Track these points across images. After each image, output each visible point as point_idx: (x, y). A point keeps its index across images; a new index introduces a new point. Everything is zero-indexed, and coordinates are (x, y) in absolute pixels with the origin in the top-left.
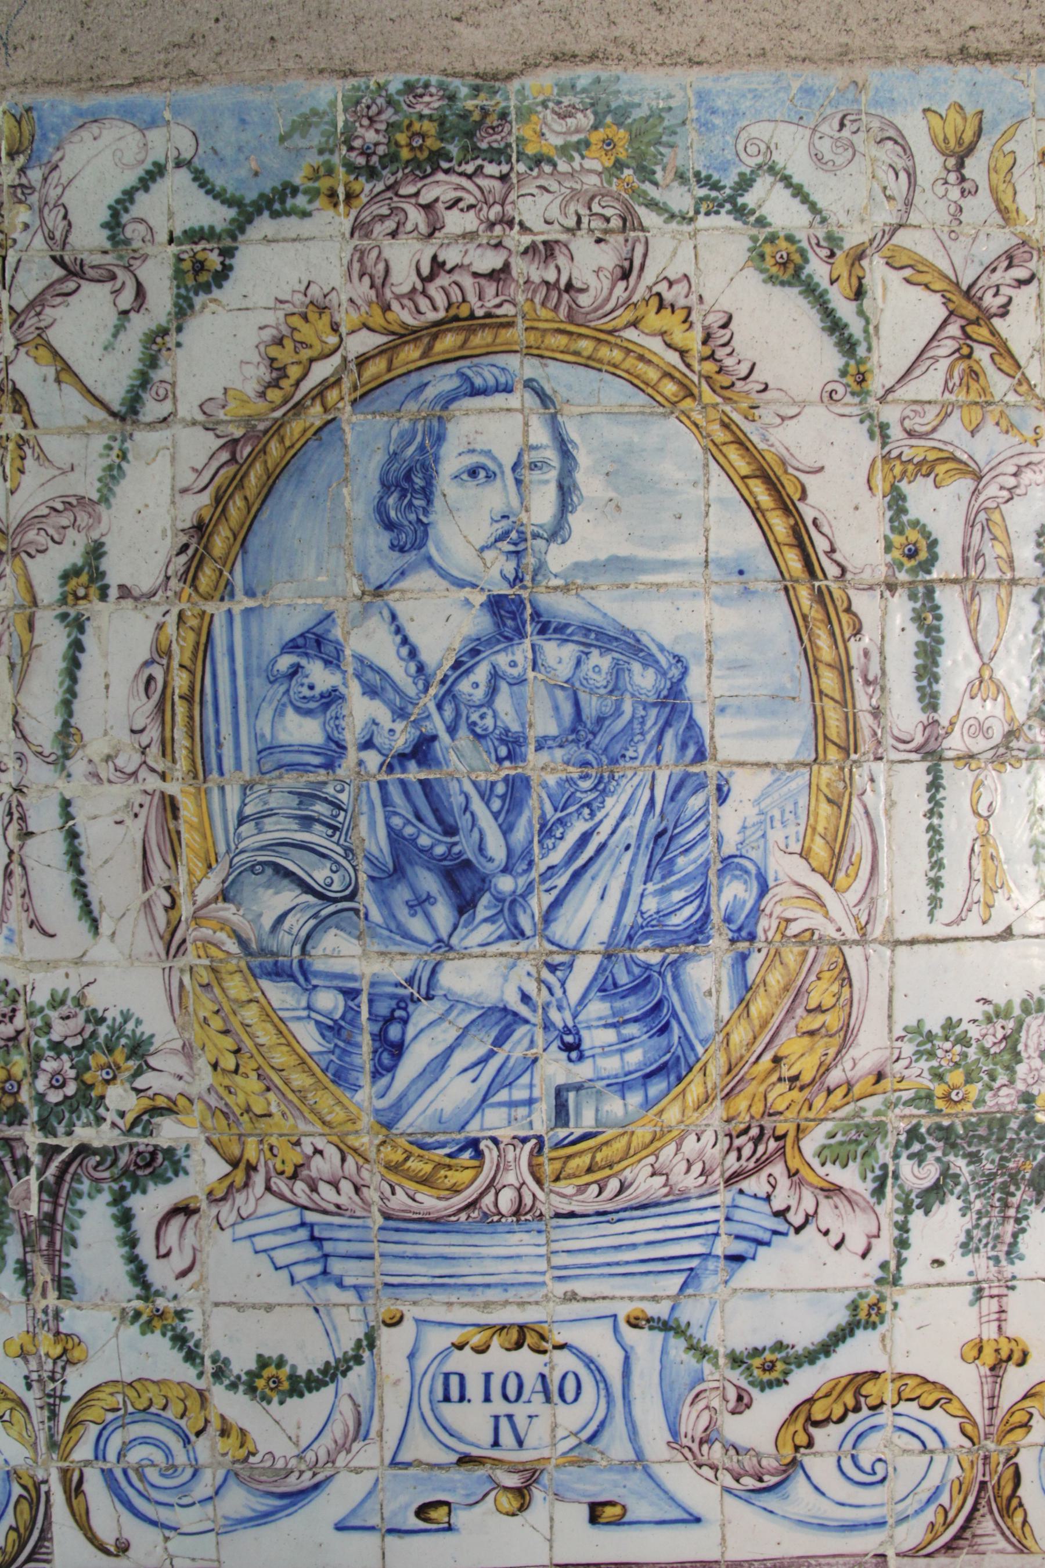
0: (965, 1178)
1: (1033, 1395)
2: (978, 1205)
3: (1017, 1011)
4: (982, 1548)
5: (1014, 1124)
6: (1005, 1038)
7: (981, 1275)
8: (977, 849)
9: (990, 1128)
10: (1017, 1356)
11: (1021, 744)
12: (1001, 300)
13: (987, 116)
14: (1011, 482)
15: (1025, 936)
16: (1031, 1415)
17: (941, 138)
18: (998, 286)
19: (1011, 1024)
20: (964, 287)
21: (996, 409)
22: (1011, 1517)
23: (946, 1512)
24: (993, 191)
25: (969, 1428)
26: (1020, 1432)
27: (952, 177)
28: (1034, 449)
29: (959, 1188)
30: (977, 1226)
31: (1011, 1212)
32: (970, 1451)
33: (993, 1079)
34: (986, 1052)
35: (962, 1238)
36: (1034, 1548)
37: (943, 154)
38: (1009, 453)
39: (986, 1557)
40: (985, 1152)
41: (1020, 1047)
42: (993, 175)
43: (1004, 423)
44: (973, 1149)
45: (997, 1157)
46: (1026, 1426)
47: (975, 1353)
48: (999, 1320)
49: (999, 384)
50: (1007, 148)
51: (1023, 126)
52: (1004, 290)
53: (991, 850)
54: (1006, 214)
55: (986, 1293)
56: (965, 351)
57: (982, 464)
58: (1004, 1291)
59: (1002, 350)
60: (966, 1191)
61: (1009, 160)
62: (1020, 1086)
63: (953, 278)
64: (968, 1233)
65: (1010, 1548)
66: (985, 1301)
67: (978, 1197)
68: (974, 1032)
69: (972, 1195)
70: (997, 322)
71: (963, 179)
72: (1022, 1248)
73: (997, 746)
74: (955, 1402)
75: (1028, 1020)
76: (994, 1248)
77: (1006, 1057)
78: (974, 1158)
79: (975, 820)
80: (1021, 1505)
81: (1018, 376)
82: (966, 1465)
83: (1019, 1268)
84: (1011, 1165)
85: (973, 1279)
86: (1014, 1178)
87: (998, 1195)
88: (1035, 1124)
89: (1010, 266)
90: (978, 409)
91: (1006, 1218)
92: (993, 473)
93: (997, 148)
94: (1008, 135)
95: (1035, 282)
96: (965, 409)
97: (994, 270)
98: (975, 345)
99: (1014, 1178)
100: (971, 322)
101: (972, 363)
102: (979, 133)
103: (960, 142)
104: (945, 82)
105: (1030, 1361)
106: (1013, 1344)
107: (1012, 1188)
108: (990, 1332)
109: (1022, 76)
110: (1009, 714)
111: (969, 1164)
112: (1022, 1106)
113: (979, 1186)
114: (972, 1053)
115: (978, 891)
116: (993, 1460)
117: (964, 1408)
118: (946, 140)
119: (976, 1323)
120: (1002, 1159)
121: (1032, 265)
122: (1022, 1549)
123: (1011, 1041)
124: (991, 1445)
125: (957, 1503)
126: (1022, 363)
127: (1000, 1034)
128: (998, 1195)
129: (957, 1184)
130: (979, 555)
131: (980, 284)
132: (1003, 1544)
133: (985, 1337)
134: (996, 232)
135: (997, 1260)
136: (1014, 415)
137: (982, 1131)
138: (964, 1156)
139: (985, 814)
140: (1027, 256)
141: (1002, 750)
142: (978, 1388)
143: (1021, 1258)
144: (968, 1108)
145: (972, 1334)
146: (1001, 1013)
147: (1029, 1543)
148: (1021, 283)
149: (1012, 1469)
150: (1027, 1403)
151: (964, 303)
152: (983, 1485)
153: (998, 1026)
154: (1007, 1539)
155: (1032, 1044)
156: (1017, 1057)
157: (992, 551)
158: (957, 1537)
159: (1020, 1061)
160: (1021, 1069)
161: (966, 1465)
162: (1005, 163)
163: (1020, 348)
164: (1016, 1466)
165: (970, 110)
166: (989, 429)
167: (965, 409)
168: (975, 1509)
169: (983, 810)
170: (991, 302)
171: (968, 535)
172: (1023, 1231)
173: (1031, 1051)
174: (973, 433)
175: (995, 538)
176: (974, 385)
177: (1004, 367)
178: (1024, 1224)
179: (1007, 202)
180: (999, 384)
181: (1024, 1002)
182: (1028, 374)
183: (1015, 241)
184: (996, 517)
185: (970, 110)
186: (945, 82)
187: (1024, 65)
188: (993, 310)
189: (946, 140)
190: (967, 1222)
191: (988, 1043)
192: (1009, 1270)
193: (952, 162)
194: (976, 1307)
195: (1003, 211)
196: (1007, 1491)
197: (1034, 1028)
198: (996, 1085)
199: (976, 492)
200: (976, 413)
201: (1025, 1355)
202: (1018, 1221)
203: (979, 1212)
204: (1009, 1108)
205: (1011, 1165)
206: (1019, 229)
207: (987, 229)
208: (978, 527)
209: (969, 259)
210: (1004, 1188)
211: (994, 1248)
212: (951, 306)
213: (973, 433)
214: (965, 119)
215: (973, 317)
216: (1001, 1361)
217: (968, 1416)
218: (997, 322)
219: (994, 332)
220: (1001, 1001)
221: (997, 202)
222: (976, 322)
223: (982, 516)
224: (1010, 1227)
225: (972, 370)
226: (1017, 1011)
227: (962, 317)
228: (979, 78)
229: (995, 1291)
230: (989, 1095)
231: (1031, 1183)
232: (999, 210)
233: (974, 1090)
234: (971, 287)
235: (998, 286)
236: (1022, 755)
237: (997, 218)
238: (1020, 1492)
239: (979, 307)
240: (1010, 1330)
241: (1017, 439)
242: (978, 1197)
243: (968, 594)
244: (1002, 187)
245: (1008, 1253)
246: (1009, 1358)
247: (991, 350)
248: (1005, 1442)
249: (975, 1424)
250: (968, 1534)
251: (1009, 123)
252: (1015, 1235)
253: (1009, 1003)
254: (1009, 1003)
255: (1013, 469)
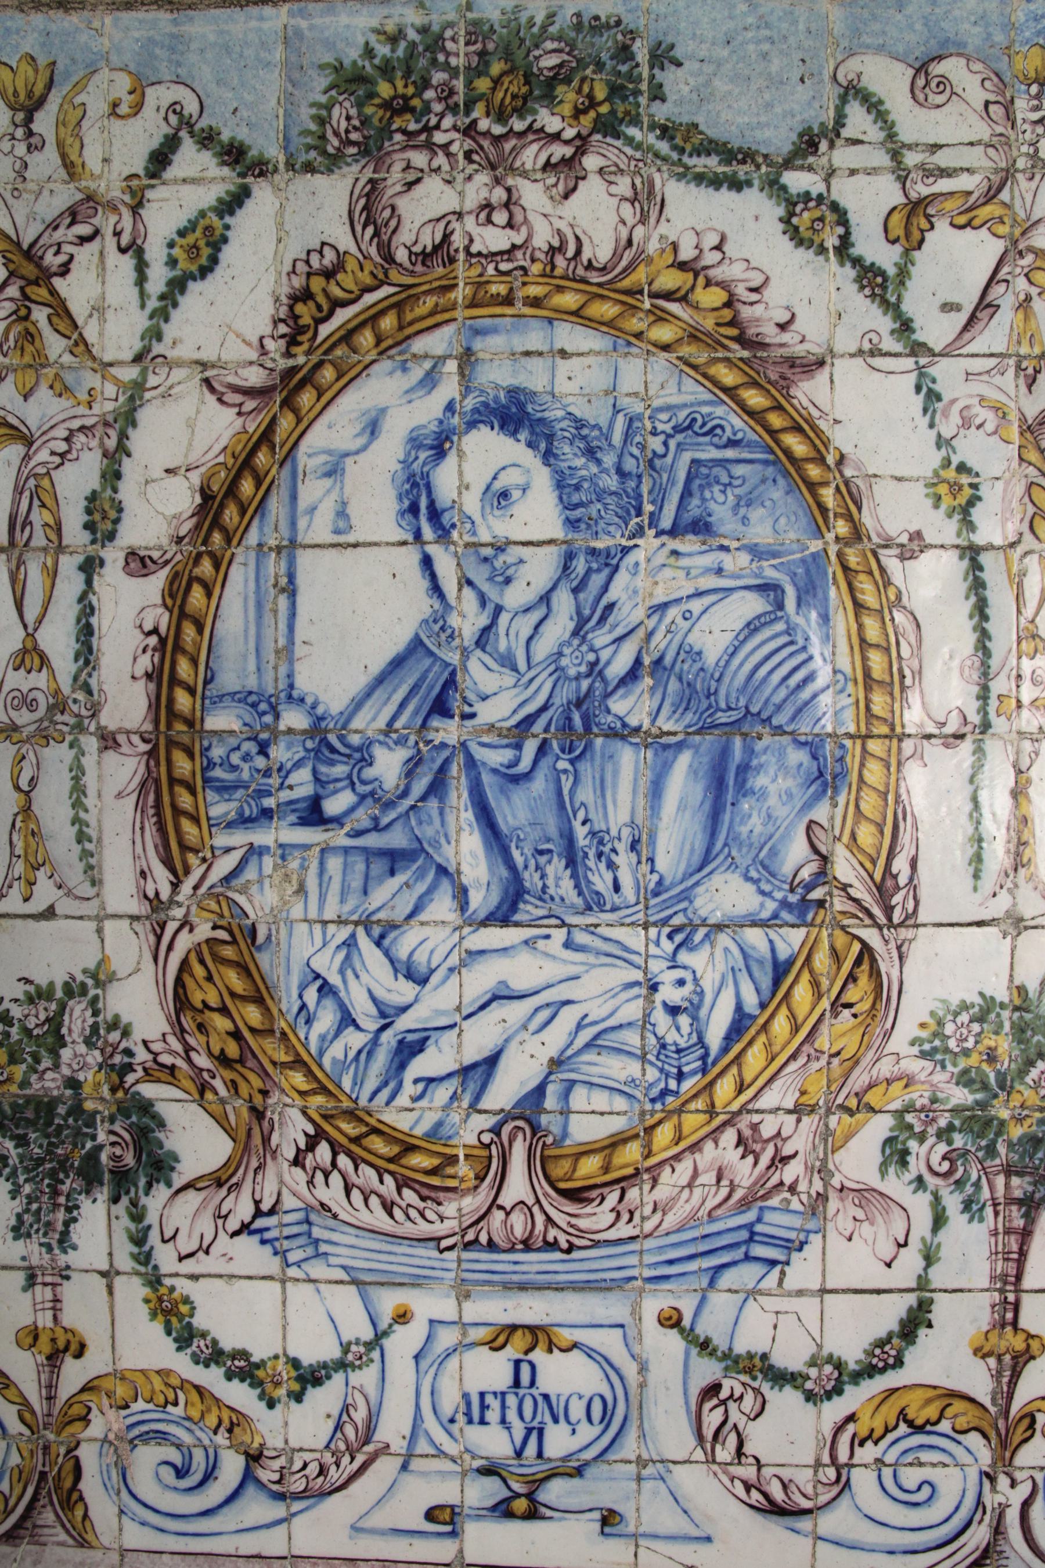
0: (14, 1160)
1: (91, 1389)
2: (27, 1189)
3: (59, 994)
4: (43, 1539)
5: (62, 1110)
6: (48, 1020)
7: (35, 1261)
8: (18, 824)
9: (37, 1111)
10: (74, 1347)
11: (66, 718)
12: (62, 258)
13: (60, 67)
14: (62, 447)
15: (67, 917)
16: (90, 1409)
17: (10, 91)
18: (59, 245)
19: (53, 1006)
20: (25, 246)
21: (50, 372)
22: (72, 1509)
23: (6, 1500)
24: (60, 145)
25: (27, 1416)
26: (79, 1425)
27: (20, 133)
28: (87, 412)
29: (7, 1170)
30: (27, 1211)
31: (62, 1200)
32: (29, 1440)
33: (37, 1060)
34: (27, 1032)
35: (13, 1222)
36: (95, 1543)
37: (12, 108)
38: (61, 417)
39: (47, 1549)
40: (33, 1136)
41: (64, 1031)
42: (62, 129)
43: (58, 386)
44: (21, 1131)
45: (45, 1143)
46: (85, 1419)
47: (29, 1340)
48: (54, 1308)
49: (55, 345)
50: (78, 100)
51: (96, 78)
52: (67, 248)
53: (32, 826)
54: (71, 169)
55: (39, 1280)
56: (23, 312)
57: (33, 429)
58: (58, 1280)
59: (60, 310)
60: (14, 1173)
61: (79, 112)
62: (66, 1071)
63: (12, 233)
64: (19, 1216)
65: (71, 1541)
66: (38, 1288)
67: (26, 1181)
68: (16, 1012)
69: (21, 1179)
70: (57, 282)
71: (30, 134)
72: (74, 1238)
73: (41, 720)
74: (13, 1389)
75: (71, 1003)
76: (45, 1234)
77: (50, 1040)
78: (22, 1141)
79: (16, 795)
80: (81, 1498)
81: (75, 336)
82: (26, 1454)
83: (72, 1258)
84: (60, 1151)
85: (26, 1264)
86: (63, 1164)
87: (47, 1181)
88: (83, 1111)
89: (72, 223)
90: (31, 372)
91: (56, 1206)
92: (45, 438)
93: (67, 100)
94: (80, 86)
95: (98, 239)
96: (20, 373)
97: (56, 228)
98: (33, 306)
99: (63, 1164)
100: (30, 283)
101: (28, 325)
102: (50, 85)
103: (30, 94)
104: (18, 32)
105: (88, 1354)
106: (70, 1335)
107: (61, 1176)
108: (45, 1320)
109: (96, 24)
110: (53, 686)
111: (16, 1147)
112: (69, 1092)
113: (27, 1170)
114: (14, 1031)
115: (19, 868)
116: (54, 1448)
117: (21, 1394)
118: (16, 93)
119: (30, 1310)
120: (50, 1144)
121: (96, 221)
122: (82, 1543)
123: (55, 1023)
124: (51, 1437)
125: (17, 1491)
126: (80, 323)
127: (42, 1016)
128: (47, 1181)
129: (6, 1165)
130: (27, 522)
131: (41, 242)
132: (63, 1537)
133: (40, 1324)
134: (57, 186)
135: (49, 1248)
136: (69, 378)
137: (30, 1114)
138: (12, 1138)
139: (26, 788)
140: (91, 212)
141: (46, 724)
142: (35, 1376)
143: (75, 1248)
144: (14, 1089)
145: (28, 1321)
146: (39, 995)
147: (90, 1537)
148: (83, 240)
149: (72, 1462)
150: (85, 1397)
151: (25, 263)
152: (43, 1475)
153: (41, 1008)
154: (67, 1532)
155: (76, 1028)
156: (61, 1042)
157: (39, 517)
158: (18, 1525)
159: (64, 1045)
160: (66, 1054)
161: (26, 1454)
162: (73, 116)
163: (78, 308)
164: (77, 1459)
165: (42, 61)
166: (43, 393)
167: (20, 373)
168: (35, 1498)
169: (24, 784)
170: (52, 260)
171: (16, 503)
172: (75, 1220)
173: (75, 1036)
174: (26, 397)
175: (43, 505)
176: (29, 348)
177: (61, 328)
178: (75, 1213)
179: (74, 157)
180: (55, 345)
181: (66, 984)
182: (86, 335)
183: (79, 196)
184: (45, 483)
185: (42, 61)
186: (18, 32)
187: (98, 12)
188: (54, 269)
189: (16, 93)
190: (17, 1205)
191: (31, 1023)
192: (62, 1259)
193: (20, 116)
194: (29, 1294)
195: (68, 165)
196: (68, 1484)
197: (77, 1013)
198: (41, 1068)
199: (26, 458)
200: (30, 378)
201: (82, 1347)
202: (69, 1210)
203: (28, 1196)
204: (55, 1093)
205: (60, 1151)
206: (84, 183)
207: (51, 186)
208: (27, 494)
209: (32, 217)
210: (53, 1174)
211: (45, 1234)
212: (12, 267)
213: (26, 397)
214: (36, 71)
215: (33, 277)
216: (58, 1351)
217: (26, 1403)
218: (57, 282)
219: (53, 292)
220: (43, 982)
221: (63, 156)
222: (36, 283)
223: (32, 482)
224: (61, 1215)
225: (28, 332)
226: (59, 994)
227: (22, 278)
228: (53, 27)
229: (48, 1279)
230: (34, 1077)
231: (80, 1173)
232: (65, 166)
233: (19, 1071)
234: (32, 245)
235: (59, 245)
236: (66, 729)
237: (63, 173)
238: (82, 1486)
239: (39, 266)
240: (67, 1320)
241: (72, 402)
242: (26, 1181)
243: (14, 562)
244: (69, 141)
245: (61, 1242)
246: (66, 1349)
247: (50, 311)
248: (64, 1434)
249: (33, 1412)
250: (29, 1524)
251: (82, 74)
252: (67, 1224)
253: (51, 984)
254: (51, 984)
255: (66, 434)
